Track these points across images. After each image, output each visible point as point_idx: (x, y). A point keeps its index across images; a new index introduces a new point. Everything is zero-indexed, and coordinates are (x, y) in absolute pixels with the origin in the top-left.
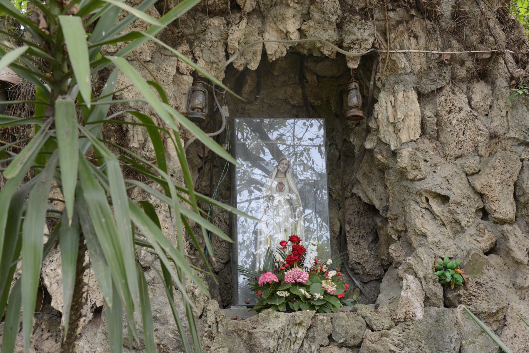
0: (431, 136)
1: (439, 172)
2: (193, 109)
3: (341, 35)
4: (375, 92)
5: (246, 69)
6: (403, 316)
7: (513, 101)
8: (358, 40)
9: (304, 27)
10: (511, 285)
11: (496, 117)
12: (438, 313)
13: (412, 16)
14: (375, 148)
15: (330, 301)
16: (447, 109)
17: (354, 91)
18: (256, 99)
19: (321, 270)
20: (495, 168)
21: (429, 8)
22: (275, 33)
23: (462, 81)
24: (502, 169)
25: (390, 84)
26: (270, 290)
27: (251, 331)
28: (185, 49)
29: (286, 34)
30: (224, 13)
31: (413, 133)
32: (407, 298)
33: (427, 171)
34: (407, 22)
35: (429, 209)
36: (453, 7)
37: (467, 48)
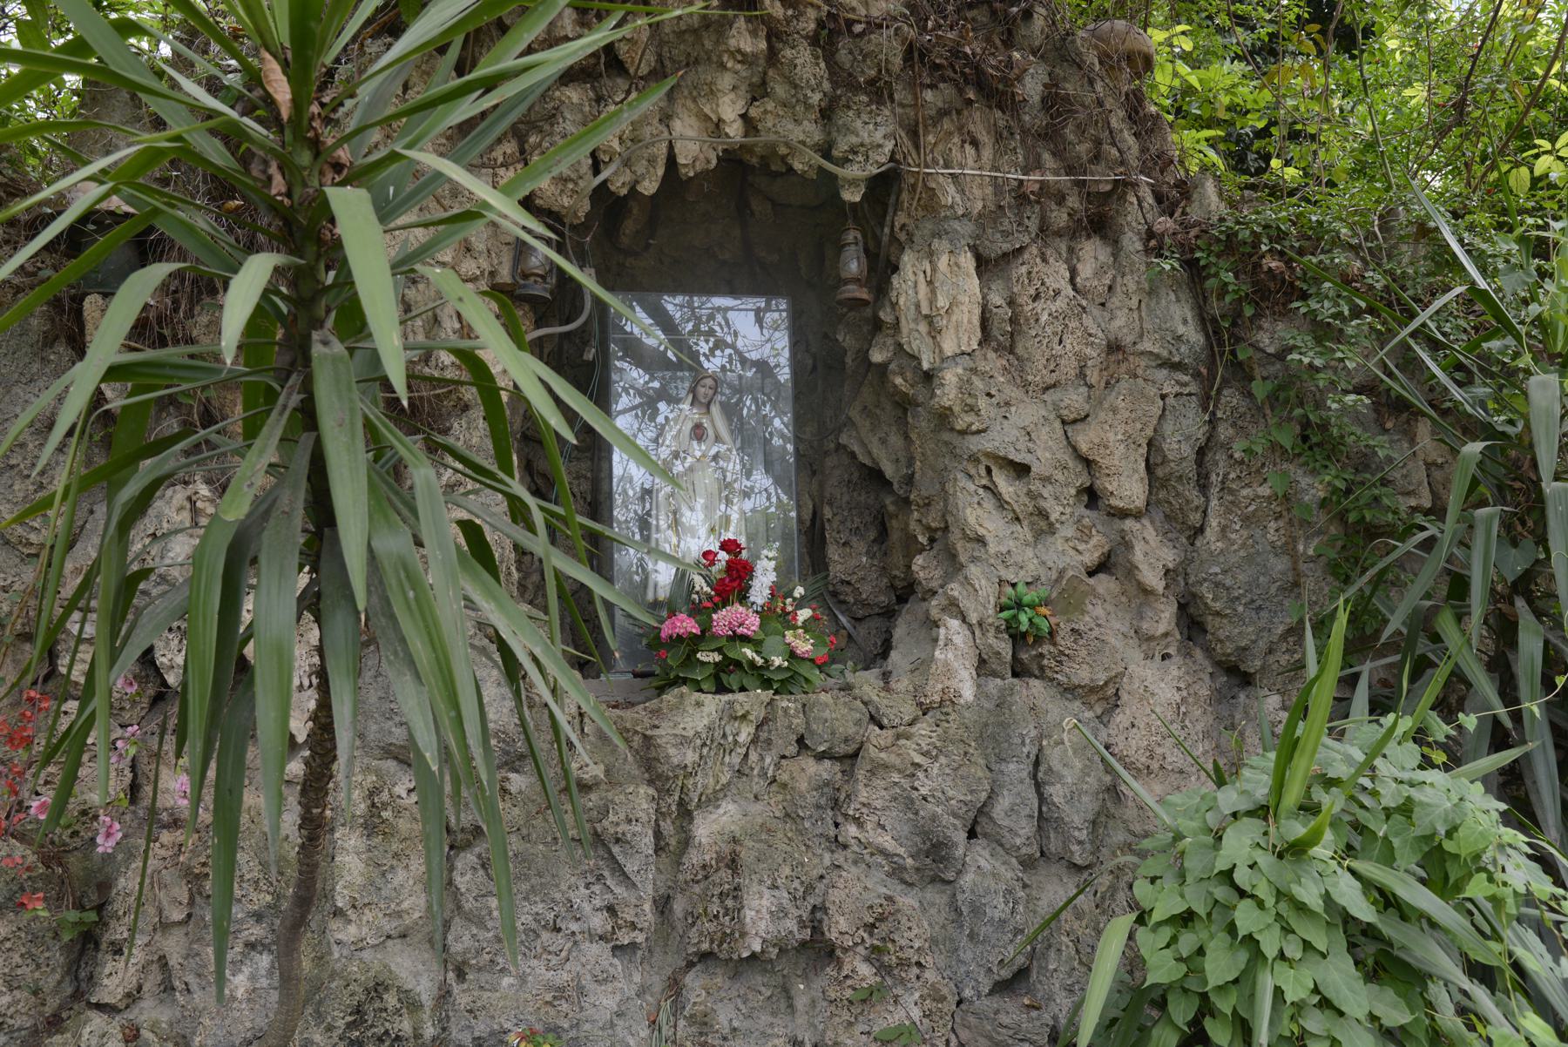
0: (999, 344)
1: (1013, 418)
2: (525, 276)
3: (829, 133)
4: (892, 249)
5: (633, 190)
6: (937, 698)
7: (1151, 281)
8: (862, 145)
9: (753, 112)
10: (1132, 633)
11: (1120, 308)
12: (1001, 690)
13: (969, 102)
14: (890, 362)
15: (801, 671)
16: (1032, 292)
17: (853, 247)
18: (648, 246)
19: (783, 609)
20: (1115, 411)
21: (1001, 87)
22: (693, 121)
23: (1059, 234)
24: (1127, 414)
25: (922, 237)
26: (683, 649)
27: (649, 733)
28: (509, 151)
29: (717, 125)
30: (589, 75)
31: (965, 339)
32: (946, 664)
33: (992, 415)
34: (959, 112)
35: (991, 489)
36: (1045, 85)
37: (1070, 170)
